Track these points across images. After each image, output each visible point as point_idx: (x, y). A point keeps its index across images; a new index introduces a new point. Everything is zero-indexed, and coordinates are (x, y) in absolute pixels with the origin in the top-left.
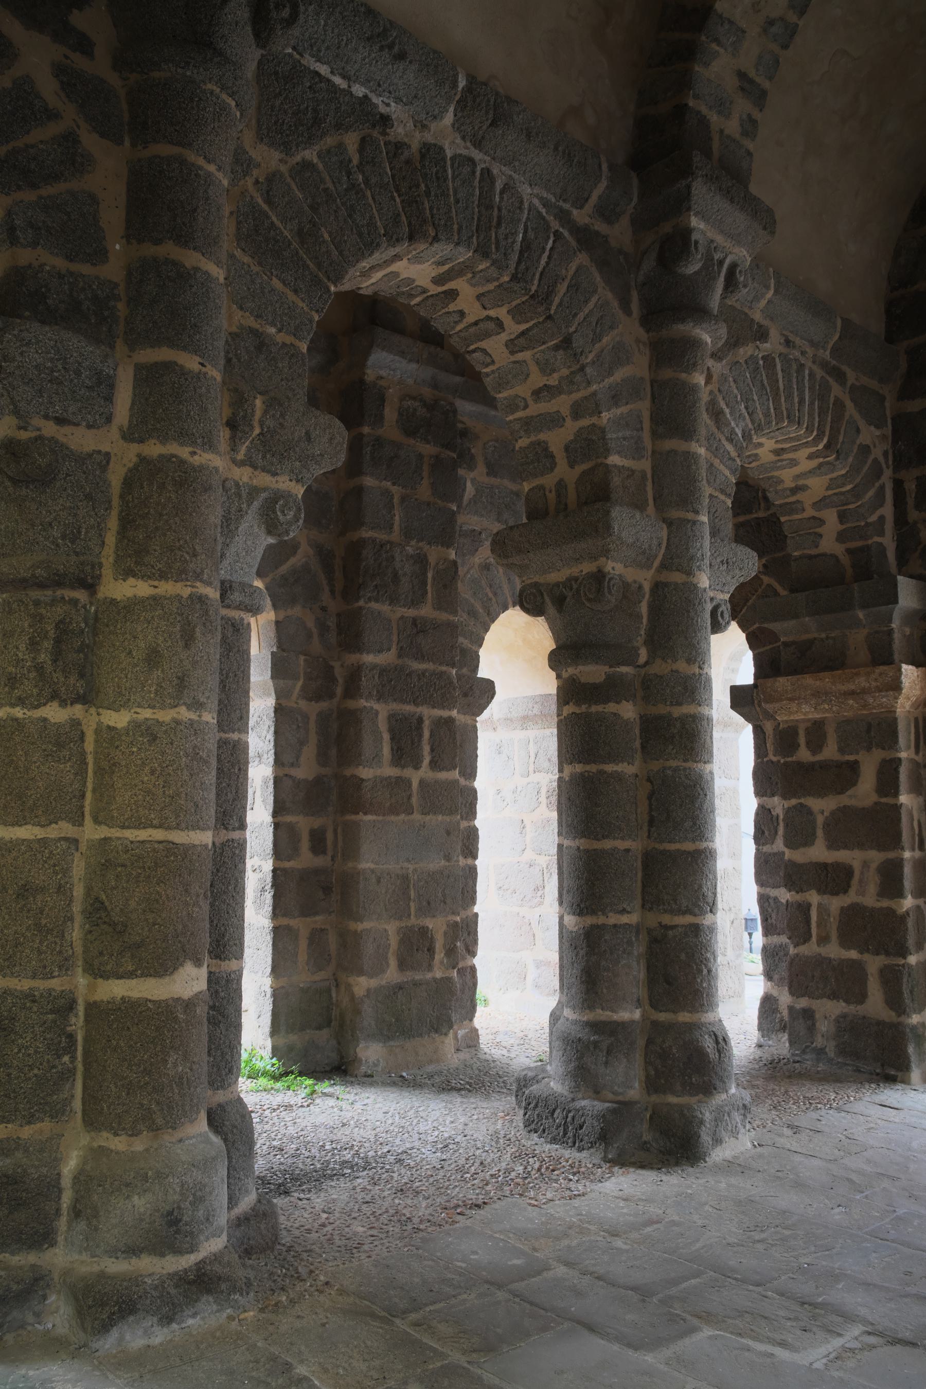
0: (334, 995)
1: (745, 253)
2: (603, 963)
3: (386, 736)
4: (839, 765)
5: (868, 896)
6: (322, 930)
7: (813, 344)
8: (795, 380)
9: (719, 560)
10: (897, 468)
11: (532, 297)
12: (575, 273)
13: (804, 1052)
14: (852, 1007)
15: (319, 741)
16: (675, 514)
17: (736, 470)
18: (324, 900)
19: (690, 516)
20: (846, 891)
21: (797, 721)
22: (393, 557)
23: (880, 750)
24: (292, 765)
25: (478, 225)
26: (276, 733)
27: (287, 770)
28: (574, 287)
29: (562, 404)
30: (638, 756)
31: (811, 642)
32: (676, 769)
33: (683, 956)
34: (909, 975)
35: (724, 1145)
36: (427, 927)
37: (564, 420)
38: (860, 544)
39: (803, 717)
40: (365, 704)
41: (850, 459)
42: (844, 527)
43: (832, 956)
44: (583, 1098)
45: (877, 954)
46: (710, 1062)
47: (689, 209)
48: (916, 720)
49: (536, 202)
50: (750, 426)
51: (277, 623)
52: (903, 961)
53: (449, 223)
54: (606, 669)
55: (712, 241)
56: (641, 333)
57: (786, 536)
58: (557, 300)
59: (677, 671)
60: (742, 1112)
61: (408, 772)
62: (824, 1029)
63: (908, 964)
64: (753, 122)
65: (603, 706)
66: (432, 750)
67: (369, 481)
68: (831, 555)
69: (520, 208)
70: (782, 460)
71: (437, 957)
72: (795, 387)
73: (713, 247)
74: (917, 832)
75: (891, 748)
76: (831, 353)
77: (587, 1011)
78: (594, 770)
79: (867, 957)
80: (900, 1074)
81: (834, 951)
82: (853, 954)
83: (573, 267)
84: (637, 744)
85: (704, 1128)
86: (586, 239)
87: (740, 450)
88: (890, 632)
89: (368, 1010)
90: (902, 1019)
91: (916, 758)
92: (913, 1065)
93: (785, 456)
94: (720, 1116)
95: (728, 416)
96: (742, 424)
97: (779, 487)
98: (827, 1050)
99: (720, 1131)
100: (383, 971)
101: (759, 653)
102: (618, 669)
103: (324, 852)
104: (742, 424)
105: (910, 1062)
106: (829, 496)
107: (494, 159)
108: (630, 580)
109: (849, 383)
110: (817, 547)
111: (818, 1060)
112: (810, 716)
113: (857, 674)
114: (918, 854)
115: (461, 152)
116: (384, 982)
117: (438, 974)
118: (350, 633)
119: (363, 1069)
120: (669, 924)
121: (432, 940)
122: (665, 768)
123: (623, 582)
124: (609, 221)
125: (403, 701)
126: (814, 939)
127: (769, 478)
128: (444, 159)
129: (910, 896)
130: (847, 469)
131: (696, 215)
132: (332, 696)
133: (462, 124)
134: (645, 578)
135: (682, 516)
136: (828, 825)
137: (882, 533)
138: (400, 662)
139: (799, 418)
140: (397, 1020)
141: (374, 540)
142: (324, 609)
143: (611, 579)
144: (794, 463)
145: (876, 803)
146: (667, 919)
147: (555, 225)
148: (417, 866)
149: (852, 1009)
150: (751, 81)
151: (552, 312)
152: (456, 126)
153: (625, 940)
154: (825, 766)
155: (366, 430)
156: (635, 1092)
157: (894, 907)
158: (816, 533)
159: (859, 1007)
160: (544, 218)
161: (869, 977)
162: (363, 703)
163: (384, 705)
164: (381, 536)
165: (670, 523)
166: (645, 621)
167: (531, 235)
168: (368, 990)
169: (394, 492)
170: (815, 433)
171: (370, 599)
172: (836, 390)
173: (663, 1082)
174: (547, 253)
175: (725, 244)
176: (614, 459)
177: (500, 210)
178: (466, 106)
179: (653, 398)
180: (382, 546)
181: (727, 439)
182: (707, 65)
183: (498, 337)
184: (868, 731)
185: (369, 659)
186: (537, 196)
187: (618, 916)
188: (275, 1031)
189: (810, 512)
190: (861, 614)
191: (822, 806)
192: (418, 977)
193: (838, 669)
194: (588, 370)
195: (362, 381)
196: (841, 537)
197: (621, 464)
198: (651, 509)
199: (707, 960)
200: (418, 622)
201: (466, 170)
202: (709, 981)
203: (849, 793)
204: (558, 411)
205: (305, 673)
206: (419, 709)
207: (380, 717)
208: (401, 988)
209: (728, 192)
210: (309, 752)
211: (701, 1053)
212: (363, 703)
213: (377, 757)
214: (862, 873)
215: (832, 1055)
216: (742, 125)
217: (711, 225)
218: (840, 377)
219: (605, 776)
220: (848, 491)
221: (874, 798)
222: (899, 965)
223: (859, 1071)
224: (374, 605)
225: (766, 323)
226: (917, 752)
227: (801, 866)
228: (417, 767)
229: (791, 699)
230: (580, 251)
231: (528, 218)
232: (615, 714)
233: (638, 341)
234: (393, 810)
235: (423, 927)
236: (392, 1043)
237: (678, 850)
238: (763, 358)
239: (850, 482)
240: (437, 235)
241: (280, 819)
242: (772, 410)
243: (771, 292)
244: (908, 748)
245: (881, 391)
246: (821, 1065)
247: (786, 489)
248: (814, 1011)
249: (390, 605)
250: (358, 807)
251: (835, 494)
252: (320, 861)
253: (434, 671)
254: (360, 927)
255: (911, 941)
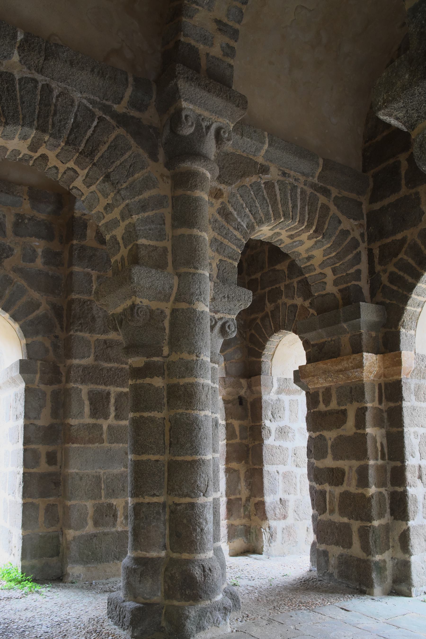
0: (61, 539)
1: (228, 121)
2: (142, 524)
3: (87, 403)
4: (338, 412)
5: (351, 486)
6: (53, 505)
7: (303, 174)
8: (289, 195)
9: (221, 296)
10: (369, 242)
11: (81, 153)
12: (114, 140)
13: (324, 575)
14: (345, 550)
15: (52, 405)
16: (183, 270)
17: (241, 245)
18: (55, 489)
19: (192, 270)
20: (342, 484)
21: (318, 388)
22: (92, 308)
23: (356, 403)
24: (35, 418)
25: (38, 115)
26: (25, 402)
27: (32, 421)
28: (113, 147)
29: (116, 214)
30: (166, 407)
31: (324, 343)
32: (182, 414)
33: (185, 521)
34: (374, 532)
35: (207, 630)
36: (113, 504)
37: (119, 222)
38: (345, 286)
39: (321, 386)
40: (73, 385)
41: (334, 238)
42: (336, 277)
43: (336, 521)
44: (129, 601)
45: (357, 520)
46: (197, 583)
47: (180, 97)
48: (380, 385)
49: (85, 101)
50: (253, 220)
51: (27, 345)
52: (370, 524)
53: (16, 115)
54: (145, 359)
55: (200, 115)
56: (166, 171)
57: (310, 285)
58: (99, 155)
59: (182, 359)
60: (224, 611)
61: (100, 421)
62: (333, 562)
63: (373, 526)
64: (232, 49)
65: (143, 380)
66: (116, 409)
67: (76, 269)
68: (332, 294)
69: (72, 105)
70: (295, 242)
71: (118, 520)
72: (290, 198)
73: (201, 119)
74: (379, 449)
75: (361, 401)
76: (318, 179)
77: (134, 551)
78: (138, 416)
79: (352, 521)
80: (368, 590)
81: (337, 518)
82: (345, 520)
83: (113, 136)
84: (165, 400)
85: (189, 621)
86: (123, 120)
87: (245, 234)
88: (361, 335)
89: (74, 547)
90: (370, 557)
91: (380, 407)
92: (376, 585)
93: (296, 239)
94: (202, 614)
95: (236, 216)
96: (246, 220)
97: (300, 258)
98: (334, 574)
99: (203, 623)
100: (83, 527)
101: (308, 352)
102: (152, 359)
103: (55, 464)
104: (246, 220)
105: (373, 582)
106: (326, 260)
107: (53, 79)
108: (154, 308)
109: (333, 196)
110: (325, 289)
111: (330, 580)
112: (324, 385)
113: (343, 360)
114: (380, 462)
115: (26, 76)
116: (84, 533)
117: (120, 529)
118: (66, 349)
119: (70, 579)
120: (178, 502)
121: (116, 510)
122: (176, 414)
123: (149, 310)
124: (140, 110)
125: (97, 384)
126: (328, 511)
127: (294, 252)
128: (13, 80)
129: (374, 487)
130: (331, 243)
131: (186, 100)
132: (60, 382)
133: (26, 60)
134: (167, 307)
135: (187, 271)
136: (333, 446)
137: (359, 279)
138: (96, 363)
139: (292, 216)
140: (93, 553)
141: (79, 300)
142: (56, 337)
143: (139, 308)
144: (301, 243)
145: (355, 433)
146: (177, 500)
147: (99, 113)
148: (106, 471)
149: (345, 551)
150: (226, 25)
151: (95, 161)
152: (23, 62)
153: (155, 511)
154: (331, 413)
155: (75, 242)
156: (158, 598)
157: (365, 493)
158: (323, 282)
159: (349, 550)
160: (90, 110)
161: (353, 533)
162: (72, 385)
163: (85, 386)
164: (85, 297)
165: (179, 275)
166: (167, 331)
167: (80, 119)
168: (74, 537)
169: (92, 274)
170: (306, 224)
171: (77, 331)
172: (322, 199)
173: (171, 593)
174: (92, 129)
175: (211, 117)
176: (142, 241)
177: (55, 106)
178: (24, 50)
179: (173, 207)
180: (85, 303)
181: (235, 228)
182: (191, 17)
183: (78, 179)
184: (351, 392)
185: (76, 362)
186: (86, 98)
187: (151, 498)
188: (24, 557)
189: (318, 271)
190: (345, 326)
191: (330, 435)
192: (106, 530)
193: (334, 358)
194: (122, 192)
195: (73, 217)
196: (336, 283)
197: (148, 244)
198: (170, 267)
199: (200, 523)
200: (107, 342)
201: (30, 85)
202: (202, 535)
203: (342, 427)
204: (116, 218)
205: (41, 370)
206: (108, 388)
207: (83, 392)
208: (95, 536)
209: (206, 87)
210: (46, 411)
211: (192, 578)
212: (72, 385)
213: (81, 414)
214: (349, 474)
215: (336, 577)
216: (223, 51)
217: (197, 106)
218: (326, 192)
219: (144, 419)
220: (334, 256)
221: (354, 430)
222: (367, 526)
223: (349, 587)
224: (79, 333)
225: (266, 163)
226: (380, 402)
227: (321, 469)
228: (106, 417)
229: (313, 376)
230: (118, 127)
231: (78, 110)
232: (149, 384)
233: (162, 175)
234: (91, 441)
235: (110, 504)
236: (89, 565)
237: (183, 460)
238: (264, 183)
239: (334, 251)
240: (6, 121)
241: (27, 446)
242: (271, 212)
243: (266, 146)
244: (373, 401)
245: (358, 200)
246: (331, 583)
247: (304, 258)
248: (328, 552)
249: (90, 333)
250: (71, 440)
251: (328, 258)
252: (52, 469)
253: (118, 367)
254: (69, 503)
255: (374, 512)
